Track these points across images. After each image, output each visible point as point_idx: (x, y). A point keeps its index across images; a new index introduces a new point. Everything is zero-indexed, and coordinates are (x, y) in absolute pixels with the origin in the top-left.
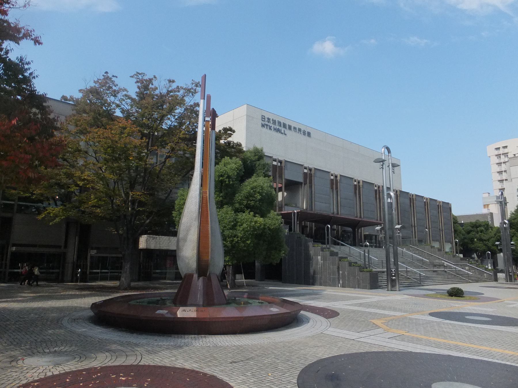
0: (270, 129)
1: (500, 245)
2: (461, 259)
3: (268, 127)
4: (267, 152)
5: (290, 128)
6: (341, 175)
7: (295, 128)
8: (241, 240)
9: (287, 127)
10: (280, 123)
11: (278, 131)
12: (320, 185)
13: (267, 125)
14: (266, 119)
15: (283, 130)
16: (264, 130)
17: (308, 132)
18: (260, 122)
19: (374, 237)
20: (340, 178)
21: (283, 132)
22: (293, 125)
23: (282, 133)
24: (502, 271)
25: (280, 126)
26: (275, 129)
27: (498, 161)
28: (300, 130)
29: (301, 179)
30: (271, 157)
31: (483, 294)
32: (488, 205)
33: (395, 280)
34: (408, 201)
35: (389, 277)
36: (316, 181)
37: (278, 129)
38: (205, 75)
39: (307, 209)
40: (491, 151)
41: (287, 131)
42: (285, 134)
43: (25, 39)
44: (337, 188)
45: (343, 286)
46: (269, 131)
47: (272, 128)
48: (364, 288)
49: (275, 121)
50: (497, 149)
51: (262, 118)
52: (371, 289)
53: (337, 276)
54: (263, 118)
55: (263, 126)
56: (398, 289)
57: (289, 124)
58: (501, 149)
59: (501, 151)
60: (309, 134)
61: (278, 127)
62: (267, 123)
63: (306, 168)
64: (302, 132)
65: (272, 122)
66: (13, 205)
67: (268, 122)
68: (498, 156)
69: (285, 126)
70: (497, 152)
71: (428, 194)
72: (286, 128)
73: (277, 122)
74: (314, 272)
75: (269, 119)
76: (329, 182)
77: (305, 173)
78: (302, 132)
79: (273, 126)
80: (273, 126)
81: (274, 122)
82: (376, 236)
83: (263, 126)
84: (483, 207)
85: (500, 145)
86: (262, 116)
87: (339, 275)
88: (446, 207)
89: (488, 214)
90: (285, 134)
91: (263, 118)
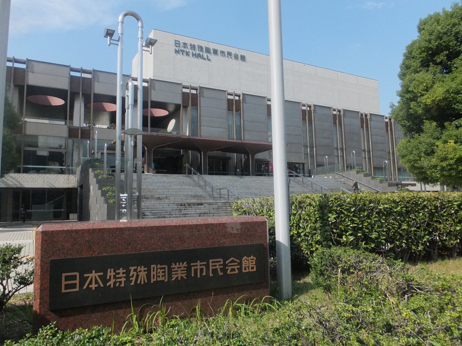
0: (187, 54)
3: (185, 54)
5: (215, 52)
6: (371, 114)
7: (222, 52)
10: (201, 48)
11: (198, 56)
13: (183, 51)
15: (205, 55)
16: (180, 56)
17: (241, 56)
18: (173, 48)
19: (301, 166)
20: (371, 116)
21: (205, 57)
22: (220, 48)
23: (205, 59)
28: (229, 54)
30: (180, 84)
34: (358, 122)
36: (203, 102)
39: (189, 135)
41: (212, 56)
42: (209, 60)
44: (367, 127)
46: (185, 57)
49: (194, 45)
51: (176, 43)
54: (177, 43)
55: (177, 52)
60: (243, 58)
61: (197, 52)
62: (182, 49)
63: (334, 110)
65: (189, 47)
66: (24, 164)
67: (185, 47)
69: (208, 50)
71: (339, 102)
72: (210, 53)
73: (197, 46)
75: (185, 44)
76: (384, 125)
77: (386, 122)
79: (191, 51)
80: (191, 51)
81: (193, 47)
82: (303, 164)
83: (177, 52)
86: (175, 41)
90: (209, 60)
91: (177, 43)
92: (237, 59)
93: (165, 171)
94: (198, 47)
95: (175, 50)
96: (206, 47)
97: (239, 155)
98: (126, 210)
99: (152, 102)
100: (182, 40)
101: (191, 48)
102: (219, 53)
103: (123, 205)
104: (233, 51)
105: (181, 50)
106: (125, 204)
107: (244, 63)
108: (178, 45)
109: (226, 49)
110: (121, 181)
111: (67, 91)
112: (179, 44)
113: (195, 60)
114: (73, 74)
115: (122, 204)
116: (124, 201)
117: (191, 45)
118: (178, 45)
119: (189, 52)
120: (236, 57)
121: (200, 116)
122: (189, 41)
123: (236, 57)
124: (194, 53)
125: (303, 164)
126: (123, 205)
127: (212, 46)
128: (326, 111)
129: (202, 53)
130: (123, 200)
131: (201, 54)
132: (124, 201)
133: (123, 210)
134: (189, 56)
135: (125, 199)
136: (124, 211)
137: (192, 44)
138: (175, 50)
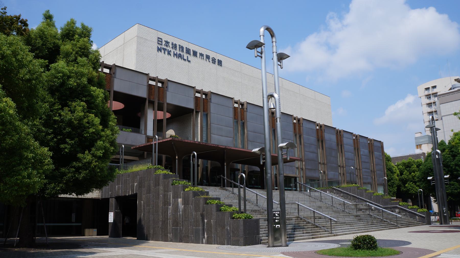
0: (169, 53)
1: (433, 180)
2: (378, 199)
3: (166, 53)
4: (54, 19)
5: (195, 54)
7: (201, 55)
8: (38, 169)
9: (192, 53)
10: (181, 48)
11: (180, 56)
12: (220, 117)
13: (165, 50)
14: (164, 43)
15: (185, 56)
16: (161, 54)
18: (156, 45)
21: (185, 58)
22: (199, 50)
23: (185, 60)
24: (435, 214)
25: (183, 51)
26: (175, 55)
27: (428, 101)
28: (208, 57)
29: (191, 105)
31: (409, 243)
32: (420, 145)
33: (278, 229)
35: (270, 225)
36: (213, 108)
37: (180, 54)
38: (289, 56)
40: (421, 92)
41: (191, 58)
42: (189, 61)
43: (21, 18)
45: (209, 242)
47: (172, 54)
48: (236, 243)
49: (176, 45)
50: (427, 89)
51: (158, 41)
52: (245, 245)
53: (201, 228)
54: (160, 40)
55: (159, 50)
56: (284, 244)
57: (213, 65)
58: (430, 89)
59: (431, 92)
60: (220, 63)
62: (165, 47)
64: (211, 60)
65: (171, 46)
67: (167, 46)
68: (428, 96)
69: (188, 51)
70: (427, 93)
72: (190, 55)
74: (140, 220)
75: (167, 43)
76: (231, 114)
78: (211, 60)
79: (172, 51)
80: (172, 51)
81: (174, 46)
82: (295, 178)
83: (159, 50)
84: (415, 147)
85: (430, 85)
86: (158, 38)
87: (204, 225)
88: (375, 147)
89: (421, 154)
90: (189, 61)
91: (160, 40)
92: (215, 63)
93: (260, 187)
94: (179, 47)
95: (158, 47)
96: (218, 60)
97: (205, 161)
98: (279, 226)
99: (116, 93)
100: (165, 38)
101: (172, 47)
102: (198, 55)
103: (276, 221)
104: (212, 55)
105: (163, 49)
106: (278, 219)
107: (220, 67)
108: (160, 43)
109: (205, 52)
110: (445, 207)
111: (146, 99)
112: (162, 42)
113: (173, 59)
114: (151, 82)
115: (276, 219)
116: (277, 217)
117: (172, 44)
118: (160, 43)
119: (171, 51)
120: (214, 61)
121: (210, 123)
122: (171, 40)
123: (214, 61)
124: (175, 53)
125: (295, 178)
126: (276, 221)
127: (192, 48)
128: (312, 126)
129: (182, 53)
130: (276, 215)
131: (182, 54)
132: (277, 217)
133: (277, 226)
134: (170, 55)
135: (278, 214)
136: (278, 227)
137: (174, 43)
138: (158, 47)
